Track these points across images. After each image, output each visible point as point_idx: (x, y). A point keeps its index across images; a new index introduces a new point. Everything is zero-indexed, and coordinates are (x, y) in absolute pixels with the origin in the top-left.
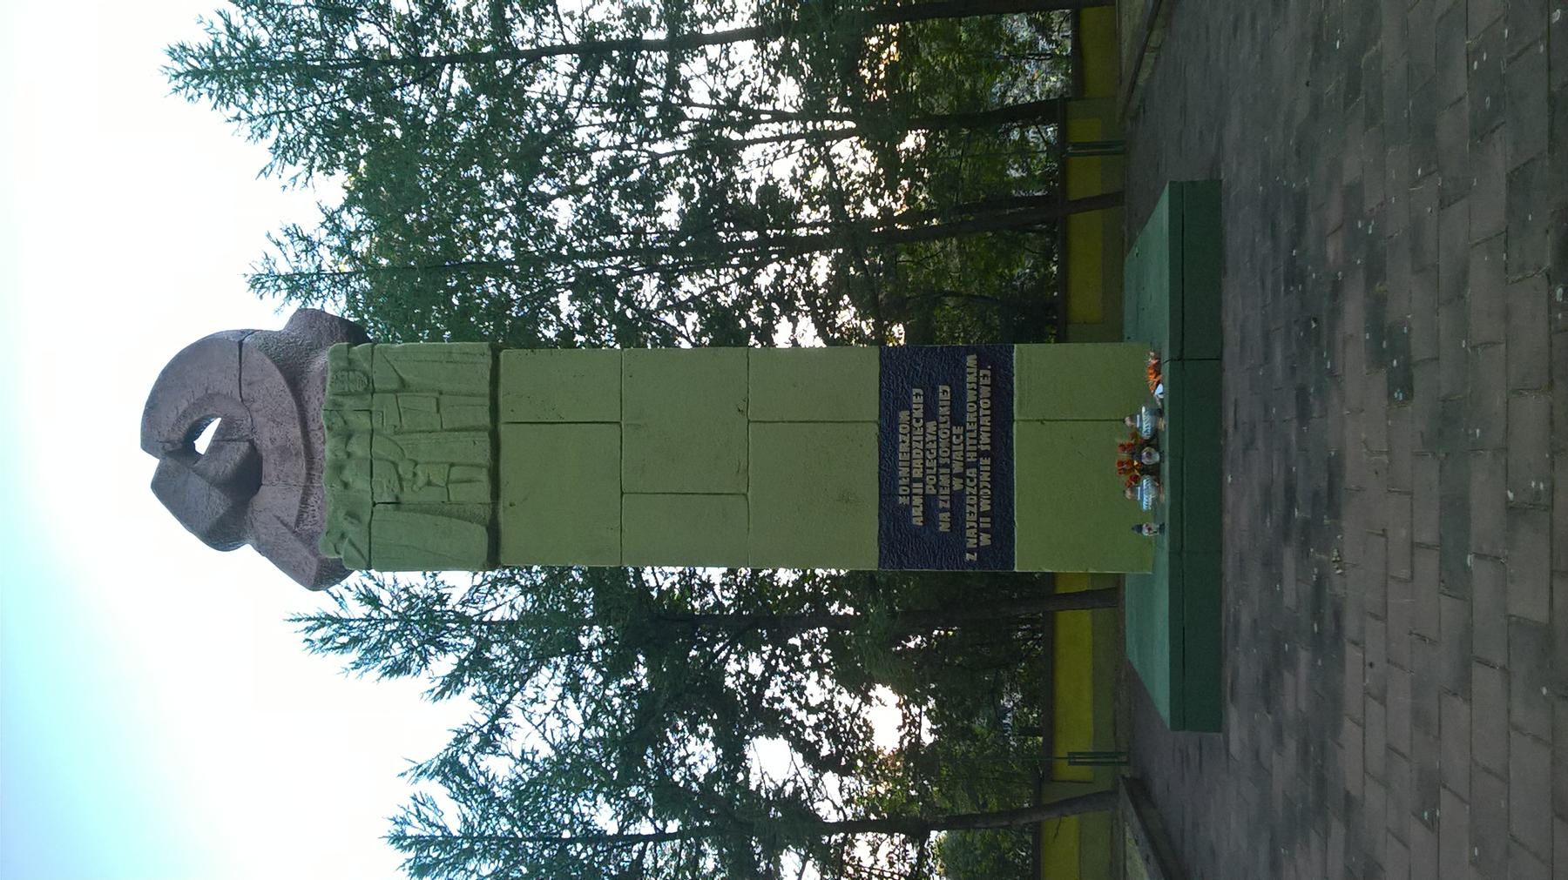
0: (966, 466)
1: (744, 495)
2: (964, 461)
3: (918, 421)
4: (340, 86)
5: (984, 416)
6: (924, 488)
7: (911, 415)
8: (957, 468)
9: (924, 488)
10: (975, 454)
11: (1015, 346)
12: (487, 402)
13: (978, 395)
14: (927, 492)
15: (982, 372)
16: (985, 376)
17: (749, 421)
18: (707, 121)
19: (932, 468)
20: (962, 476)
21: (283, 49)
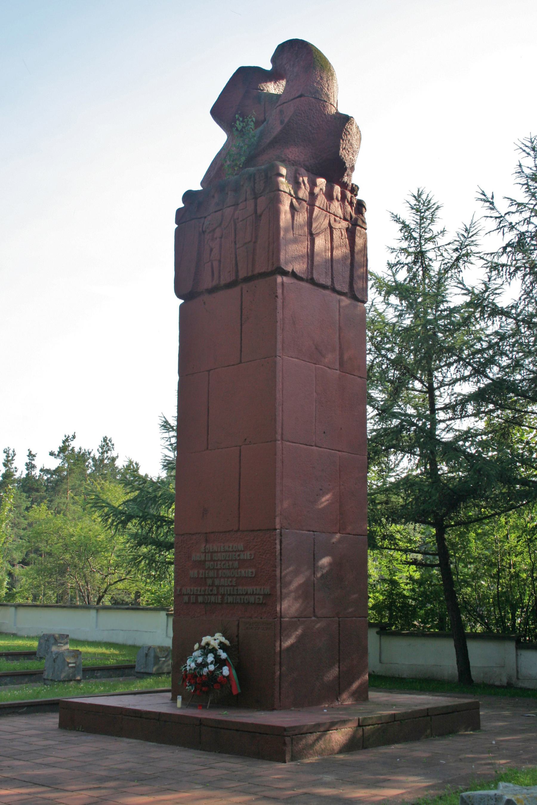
0: (218, 587)
1: (208, 448)
2: (220, 586)
3: (239, 555)
4: (371, 595)
5: (241, 599)
6: (208, 561)
7: (241, 551)
8: (217, 582)
9: (208, 561)
10: (223, 593)
11: (239, 691)
12: (250, 274)
13: (250, 594)
14: (207, 563)
15: (261, 597)
16: (259, 598)
17: (240, 446)
18: (467, 544)
19: (217, 566)
20: (213, 585)
21: (422, 226)
